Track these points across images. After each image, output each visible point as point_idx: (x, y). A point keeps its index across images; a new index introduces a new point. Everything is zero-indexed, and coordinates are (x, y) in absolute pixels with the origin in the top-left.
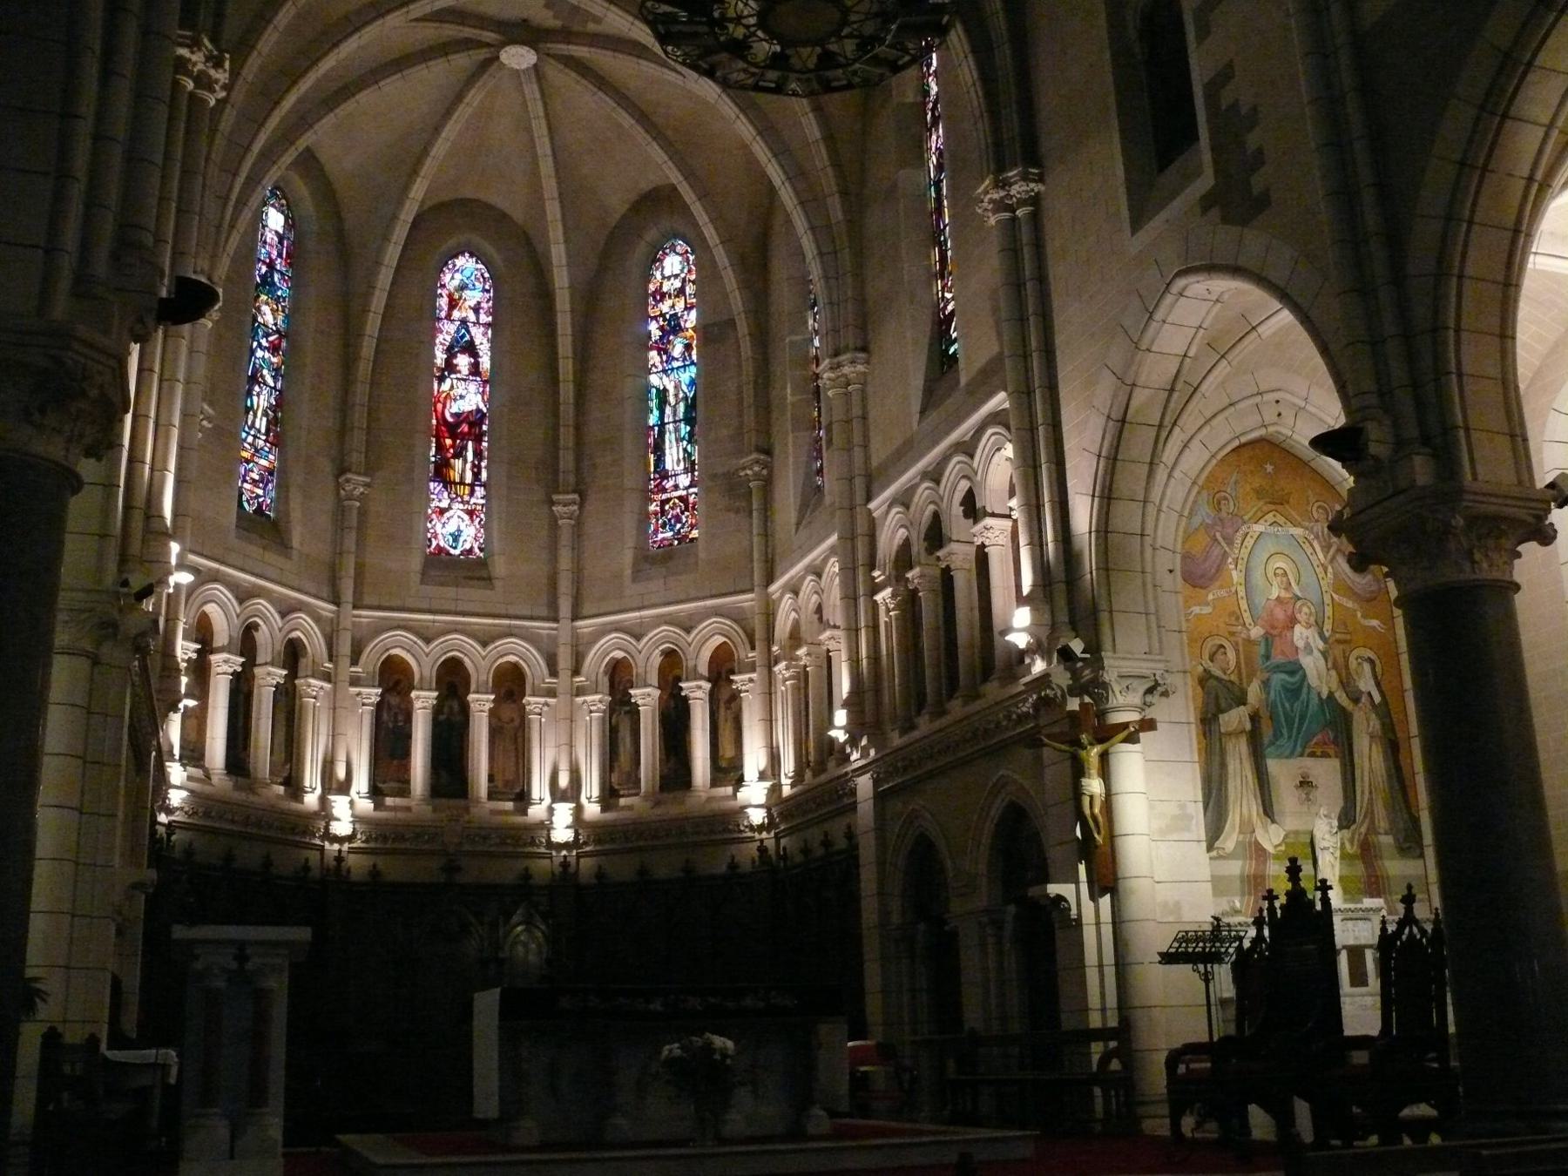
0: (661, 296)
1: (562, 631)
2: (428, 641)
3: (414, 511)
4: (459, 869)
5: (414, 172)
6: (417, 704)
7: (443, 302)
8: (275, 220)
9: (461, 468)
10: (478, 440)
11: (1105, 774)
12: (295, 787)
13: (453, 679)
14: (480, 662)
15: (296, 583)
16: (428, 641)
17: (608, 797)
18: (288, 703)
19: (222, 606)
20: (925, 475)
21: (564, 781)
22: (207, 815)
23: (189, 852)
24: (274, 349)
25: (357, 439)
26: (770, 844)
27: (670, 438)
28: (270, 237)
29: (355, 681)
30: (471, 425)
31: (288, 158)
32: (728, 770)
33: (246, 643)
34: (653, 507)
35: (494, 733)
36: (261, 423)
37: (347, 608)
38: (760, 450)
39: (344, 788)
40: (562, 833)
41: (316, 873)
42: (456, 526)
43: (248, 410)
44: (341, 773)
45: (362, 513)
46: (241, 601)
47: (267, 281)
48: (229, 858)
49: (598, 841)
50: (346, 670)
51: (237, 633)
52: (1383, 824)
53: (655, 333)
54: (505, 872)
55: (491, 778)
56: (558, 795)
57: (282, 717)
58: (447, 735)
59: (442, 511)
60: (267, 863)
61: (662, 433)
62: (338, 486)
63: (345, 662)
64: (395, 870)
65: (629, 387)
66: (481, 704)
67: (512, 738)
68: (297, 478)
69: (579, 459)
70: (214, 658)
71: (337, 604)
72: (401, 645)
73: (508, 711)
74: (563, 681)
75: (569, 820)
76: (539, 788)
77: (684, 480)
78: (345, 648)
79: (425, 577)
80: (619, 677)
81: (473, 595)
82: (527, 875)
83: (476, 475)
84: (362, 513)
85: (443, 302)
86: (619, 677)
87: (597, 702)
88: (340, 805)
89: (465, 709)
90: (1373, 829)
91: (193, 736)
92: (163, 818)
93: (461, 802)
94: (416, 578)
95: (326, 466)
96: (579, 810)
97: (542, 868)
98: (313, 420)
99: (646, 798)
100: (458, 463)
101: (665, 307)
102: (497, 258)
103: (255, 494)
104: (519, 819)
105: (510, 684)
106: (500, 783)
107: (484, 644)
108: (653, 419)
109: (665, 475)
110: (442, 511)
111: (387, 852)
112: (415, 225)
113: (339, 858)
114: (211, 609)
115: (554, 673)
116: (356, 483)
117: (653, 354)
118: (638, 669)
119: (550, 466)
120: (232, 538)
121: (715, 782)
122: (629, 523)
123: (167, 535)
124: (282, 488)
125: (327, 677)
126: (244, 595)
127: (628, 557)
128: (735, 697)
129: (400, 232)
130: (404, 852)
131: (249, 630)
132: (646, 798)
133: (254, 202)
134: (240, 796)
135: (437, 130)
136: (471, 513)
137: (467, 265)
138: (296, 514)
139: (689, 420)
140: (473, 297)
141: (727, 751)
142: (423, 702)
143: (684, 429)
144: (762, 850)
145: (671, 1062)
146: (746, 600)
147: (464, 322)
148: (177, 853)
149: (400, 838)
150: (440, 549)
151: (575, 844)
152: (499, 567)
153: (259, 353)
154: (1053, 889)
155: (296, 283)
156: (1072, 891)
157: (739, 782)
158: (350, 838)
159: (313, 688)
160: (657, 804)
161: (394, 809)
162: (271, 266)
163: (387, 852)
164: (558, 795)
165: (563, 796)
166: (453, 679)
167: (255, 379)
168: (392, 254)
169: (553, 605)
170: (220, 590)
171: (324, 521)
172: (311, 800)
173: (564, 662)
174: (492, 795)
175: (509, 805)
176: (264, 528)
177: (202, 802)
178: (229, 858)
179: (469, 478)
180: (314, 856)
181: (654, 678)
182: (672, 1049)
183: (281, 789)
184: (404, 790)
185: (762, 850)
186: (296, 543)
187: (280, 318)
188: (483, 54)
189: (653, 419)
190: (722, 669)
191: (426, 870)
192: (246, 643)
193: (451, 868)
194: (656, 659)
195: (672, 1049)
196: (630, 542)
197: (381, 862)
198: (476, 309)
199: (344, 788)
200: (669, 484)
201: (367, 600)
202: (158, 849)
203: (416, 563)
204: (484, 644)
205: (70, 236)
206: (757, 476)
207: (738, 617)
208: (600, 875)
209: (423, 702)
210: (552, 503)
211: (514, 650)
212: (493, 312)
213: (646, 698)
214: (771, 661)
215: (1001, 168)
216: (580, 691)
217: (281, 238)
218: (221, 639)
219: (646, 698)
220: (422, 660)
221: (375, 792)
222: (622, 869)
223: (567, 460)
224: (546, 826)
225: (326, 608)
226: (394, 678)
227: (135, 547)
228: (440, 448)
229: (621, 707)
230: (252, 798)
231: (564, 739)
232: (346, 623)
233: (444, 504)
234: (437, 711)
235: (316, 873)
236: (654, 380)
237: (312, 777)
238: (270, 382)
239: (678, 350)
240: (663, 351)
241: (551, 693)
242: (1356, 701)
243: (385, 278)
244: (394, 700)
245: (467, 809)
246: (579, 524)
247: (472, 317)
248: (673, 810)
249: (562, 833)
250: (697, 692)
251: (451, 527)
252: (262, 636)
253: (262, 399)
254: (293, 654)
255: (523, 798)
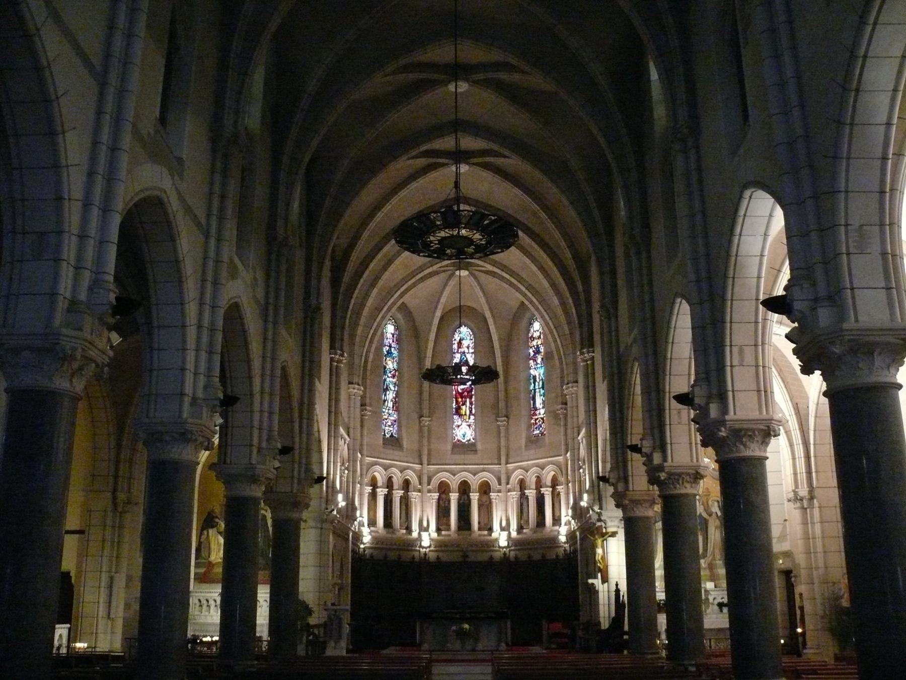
0: (533, 339)
1: (502, 468)
2: (454, 475)
3: (447, 426)
4: (467, 556)
5: (436, 307)
6: (452, 498)
7: (455, 346)
8: (390, 329)
9: (465, 409)
10: (471, 398)
11: (603, 547)
12: (409, 529)
13: (464, 488)
14: (475, 482)
15: (405, 459)
16: (454, 475)
17: (520, 529)
18: (406, 502)
19: (379, 472)
20: (537, 466)
21: (504, 524)
22: (377, 544)
23: (372, 556)
24: (393, 376)
25: (426, 404)
26: (568, 548)
27: (537, 394)
28: (389, 336)
29: (429, 491)
30: (468, 392)
31: (396, 307)
32: (557, 521)
33: (389, 484)
34: (533, 421)
35: (480, 506)
36: (390, 404)
37: (425, 465)
38: (563, 404)
39: (427, 529)
40: (503, 543)
41: (417, 559)
42: (464, 431)
43: (385, 401)
44: (425, 524)
45: (429, 431)
46: (386, 470)
47: (389, 353)
48: (386, 557)
49: (516, 546)
50: (426, 488)
51: (385, 481)
52: (718, 556)
53: (532, 354)
54: (483, 557)
55: (479, 523)
56: (502, 529)
57: (404, 507)
58: (462, 508)
59: (459, 426)
60: (400, 557)
61: (535, 392)
62: (420, 422)
63: (425, 485)
64: (445, 557)
65: (523, 376)
66: (475, 497)
67: (486, 508)
68: (404, 422)
69: (507, 402)
70: (378, 490)
71: (421, 464)
72: (444, 476)
73: (485, 498)
74: (503, 487)
75: (506, 538)
76: (496, 526)
77: (542, 411)
78: (425, 480)
79: (453, 453)
80: (522, 484)
81: (471, 457)
82: (491, 558)
83: (471, 412)
84: (429, 431)
85: (455, 346)
86: (522, 484)
87: (515, 495)
88: (425, 535)
89: (469, 500)
90: (714, 559)
91: (372, 516)
92: (362, 546)
93: (466, 532)
94: (450, 452)
95: (415, 416)
96: (510, 534)
97: (498, 555)
98: (408, 402)
99: (531, 530)
100: (464, 407)
101: (534, 343)
102: (473, 326)
103: (389, 430)
104: (489, 538)
105: (485, 489)
106: (482, 524)
107: (474, 475)
108: (532, 387)
109: (536, 410)
110: (459, 426)
111: (443, 551)
112: (442, 319)
113: (425, 554)
114: (376, 474)
115: (500, 484)
116: (426, 421)
117: (531, 361)
118: (528, 483)
119: (496, 406)
120: (381, 449)
121: (554, 525)
122: (523, 426)
123: (338, 492)
124: (399, 427)
125: (419, 491)
126: (386, 468)
127: (523, 442)
128: (559, 493)
129: (436, 322)
130: (447, 551)
131: (390, 479)
132: (531, 530)
133: (384, 322)
134: (390, 535)
135: (441, 294)
136: (469, 426)
137: (464, 330)
138: (404, 436)
139: (543, 388)
140: (465, 343)
141: (557, 514)
142: (454, 497)
143: (542, 391)
144: (565, 550)
145: (454, 631)
146: (560, 459)
147: (464, 353)
148: (368, 557)
149: (446, 546)
150: (459, 441)
151: (508, 546)
152: (479, 446)
153: (388, 379)
154: (590, 581)
155: (400, 351)
156: (597, 582)
157: (560, 525)
158: (430, 547)
159: (414, 495)
160: (535, 532)
161: (445, 535)
162: (390, 346)
163: (443, 551)
164: (502, 529)
165: (503, 531)
166: (464, 488)
167: (387, 389)
168: (432, 336)
169: (499, 458)
170: (378, 468)
171: (416, 436)
172: (415, 534)
173: (503, 481)
174: (480, 529)
175: (486, 533)
176: (393, 442)
177: (376, 540)
178: (386, 557)
179: (468, 413)
180: (416, 554)
181: (534, 486)
182: (454, 628)
183: (404, 531)
184: (448, 528)
185: (565, 550)
186: (405, 446)
187: (395, 364)
188: (450, 272)
189: (532, 387)
190: (555, 483)
191: (455, 557)
192: (389, 484)
193: (465, 556)
194: (534, 479)
195: (454, 628)
196: (524, 435)
197: (441, 554)
198: (468, 347)
199: (427, 529)
200: (537, 412)
201: (433, 461)
202: (359, 560)
203: (449, 447)
204: (474, 475)
205: (296, 473)
206: (563, 414)
207: (558, 465)
208: (516, 557)
209: (454, 497)
210: (497, 421)
211: (486, 476)
212: (475, 347)
213: (531, 493)
214: (568, 482)
215: (582, 348)
216: (509, 491)
217: (393, 335)
218: (380, 483)
219: (531, 493)
220: (454, 482)
221: (438, 530)
222: (523, 557)
223: (502, 404)
224: (497, 540)
225: (418, 467)
226: (444, 489)
227: (330, 497)
228: (457, 402)
229: (523, 497)
230: (394, 536)
231: (504, 508)
232: (425, 471)
233: (459, 423)
234: (459, 499)
235: (417, 559)
236: (532, 372)
237: (415, 526)
238: (393, 388)
239: (539, 360)
240: (535, 360)
241: (499, 491)
242: (710, 515)
243: (431, 345)
244: (443, 496)
245: (470, 535)
246: (507, 429)
247: (466, 351)
248: (539, 535)
249: (503, 543)
250: (547, 492)
251: (462, 432)
252: (395, 480)
253: (390, 395)
254: (406, 484)
255: (490, 530)
